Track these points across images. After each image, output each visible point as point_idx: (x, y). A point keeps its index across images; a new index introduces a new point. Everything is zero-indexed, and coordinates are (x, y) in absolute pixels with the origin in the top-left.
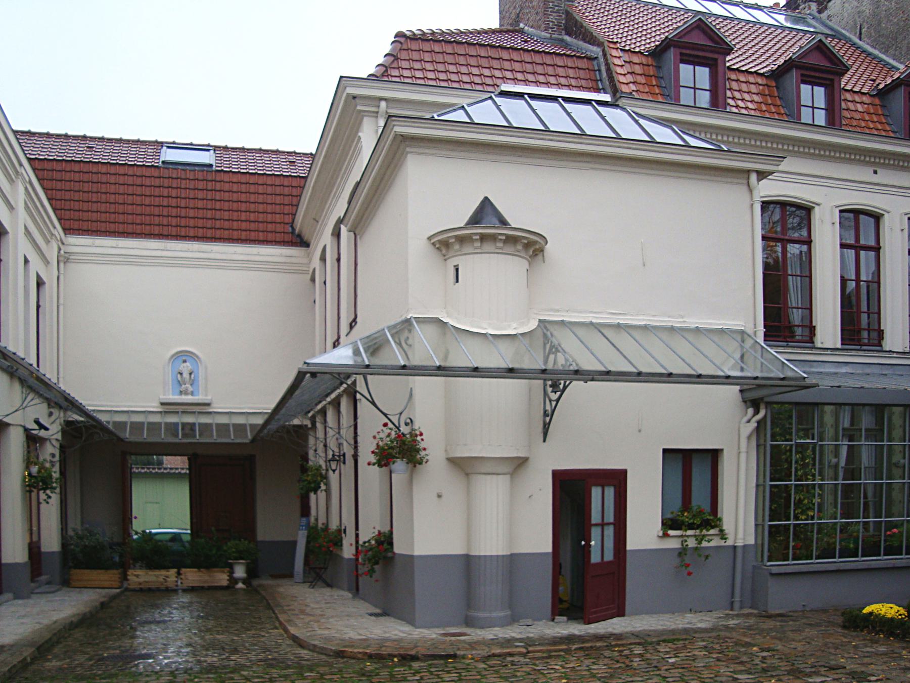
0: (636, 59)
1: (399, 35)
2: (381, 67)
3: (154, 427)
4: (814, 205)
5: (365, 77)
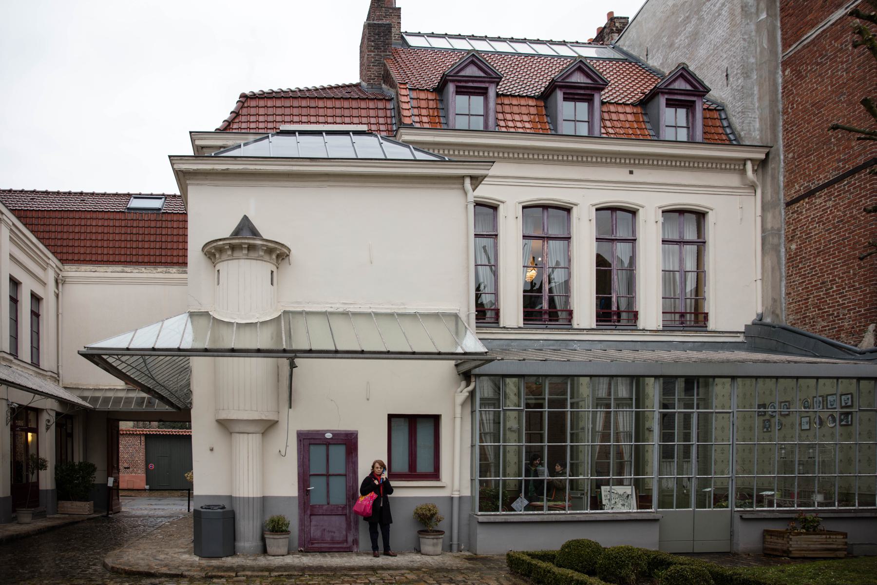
0: (423, 95)
1: (243, 96)
2: (225, 122)
3: (118, 400)
4: (707, 210)
5: (214, 131)
